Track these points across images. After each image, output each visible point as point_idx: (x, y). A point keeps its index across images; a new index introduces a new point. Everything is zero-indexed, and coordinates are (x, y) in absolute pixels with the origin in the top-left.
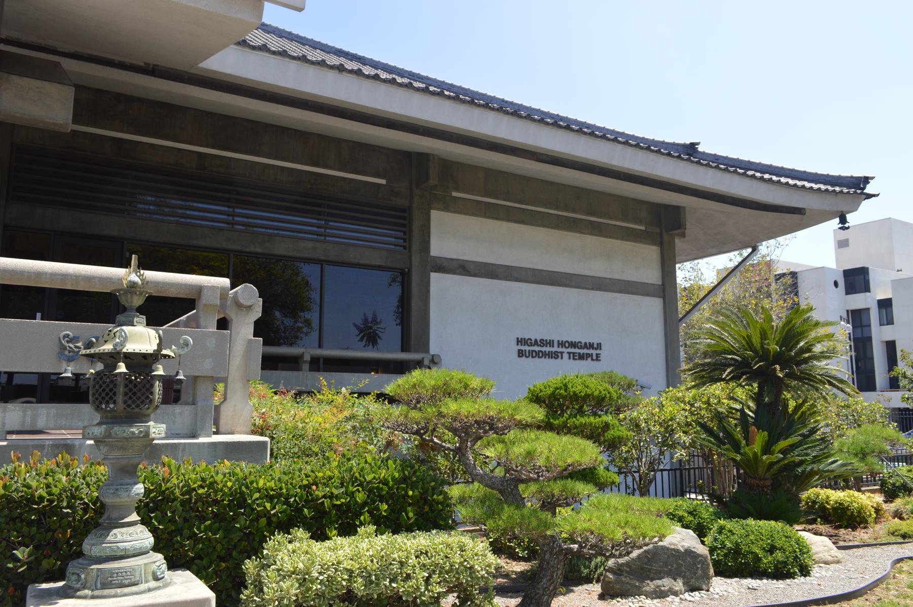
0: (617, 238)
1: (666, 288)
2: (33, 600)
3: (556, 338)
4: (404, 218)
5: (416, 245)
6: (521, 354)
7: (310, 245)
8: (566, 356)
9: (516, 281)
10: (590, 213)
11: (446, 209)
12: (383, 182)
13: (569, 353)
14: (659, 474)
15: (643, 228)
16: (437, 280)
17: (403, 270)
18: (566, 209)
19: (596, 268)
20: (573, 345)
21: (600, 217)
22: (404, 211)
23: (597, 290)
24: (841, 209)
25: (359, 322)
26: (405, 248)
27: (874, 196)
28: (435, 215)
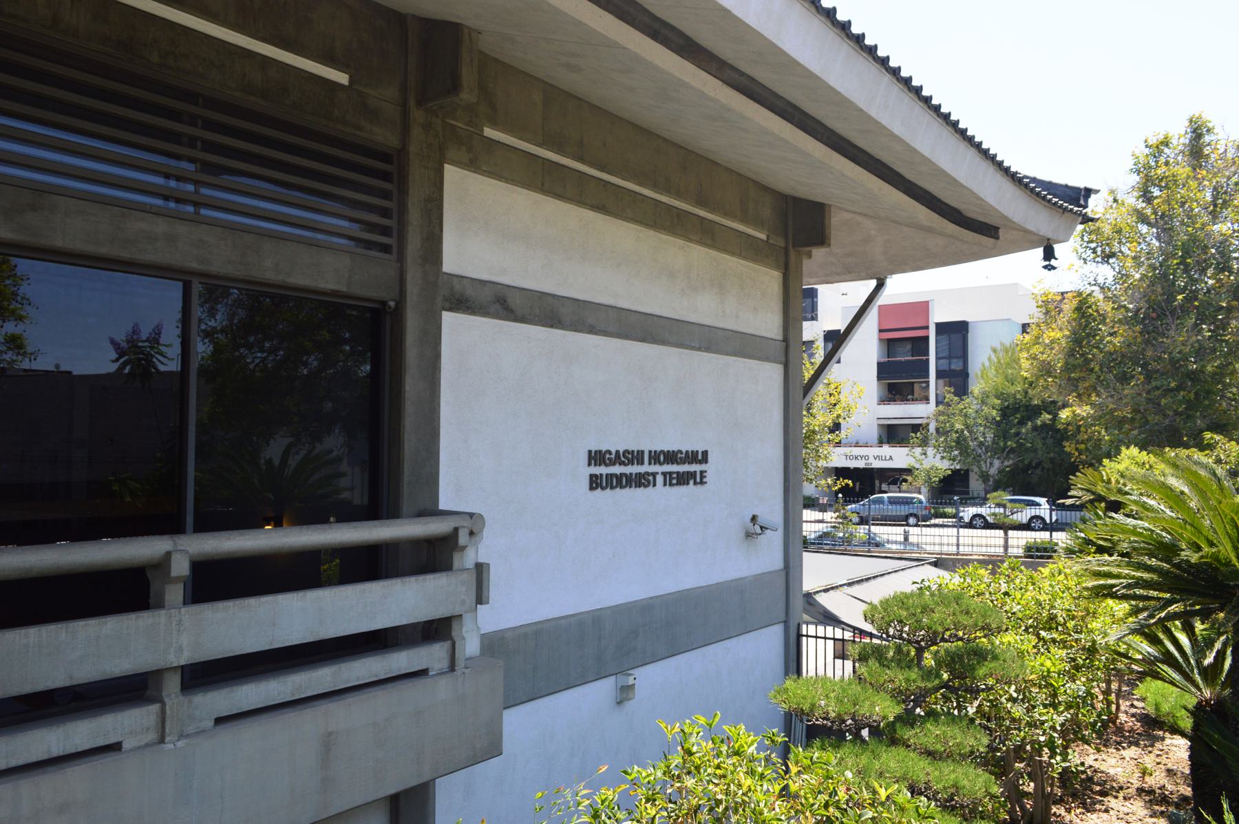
3: (647, 446)
4: (386, 176)
5: (414, 244)
6: (595, 483)
7: (160, 226)
8: (660, 479)
9: (590, 332)
10: (701, 202)
11: (472, 165)
12: (342, 78)
13: (664, 474)
15: (763, 236)
16: (459, 332)
17: (384, 303)
18: (667, 191)
19: (703, 309)
20: (671, 457)
21: (712, 211)
22: (385, 157)
24: (1050, 236)
25: (121, 337)
28: (452, 174)
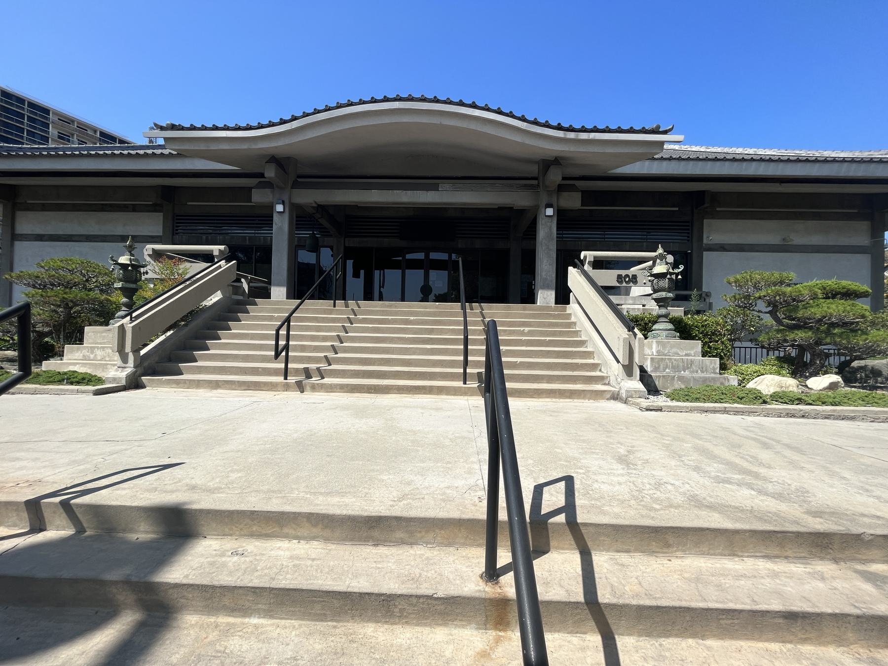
2: (839, 382)
14: (737, 350)
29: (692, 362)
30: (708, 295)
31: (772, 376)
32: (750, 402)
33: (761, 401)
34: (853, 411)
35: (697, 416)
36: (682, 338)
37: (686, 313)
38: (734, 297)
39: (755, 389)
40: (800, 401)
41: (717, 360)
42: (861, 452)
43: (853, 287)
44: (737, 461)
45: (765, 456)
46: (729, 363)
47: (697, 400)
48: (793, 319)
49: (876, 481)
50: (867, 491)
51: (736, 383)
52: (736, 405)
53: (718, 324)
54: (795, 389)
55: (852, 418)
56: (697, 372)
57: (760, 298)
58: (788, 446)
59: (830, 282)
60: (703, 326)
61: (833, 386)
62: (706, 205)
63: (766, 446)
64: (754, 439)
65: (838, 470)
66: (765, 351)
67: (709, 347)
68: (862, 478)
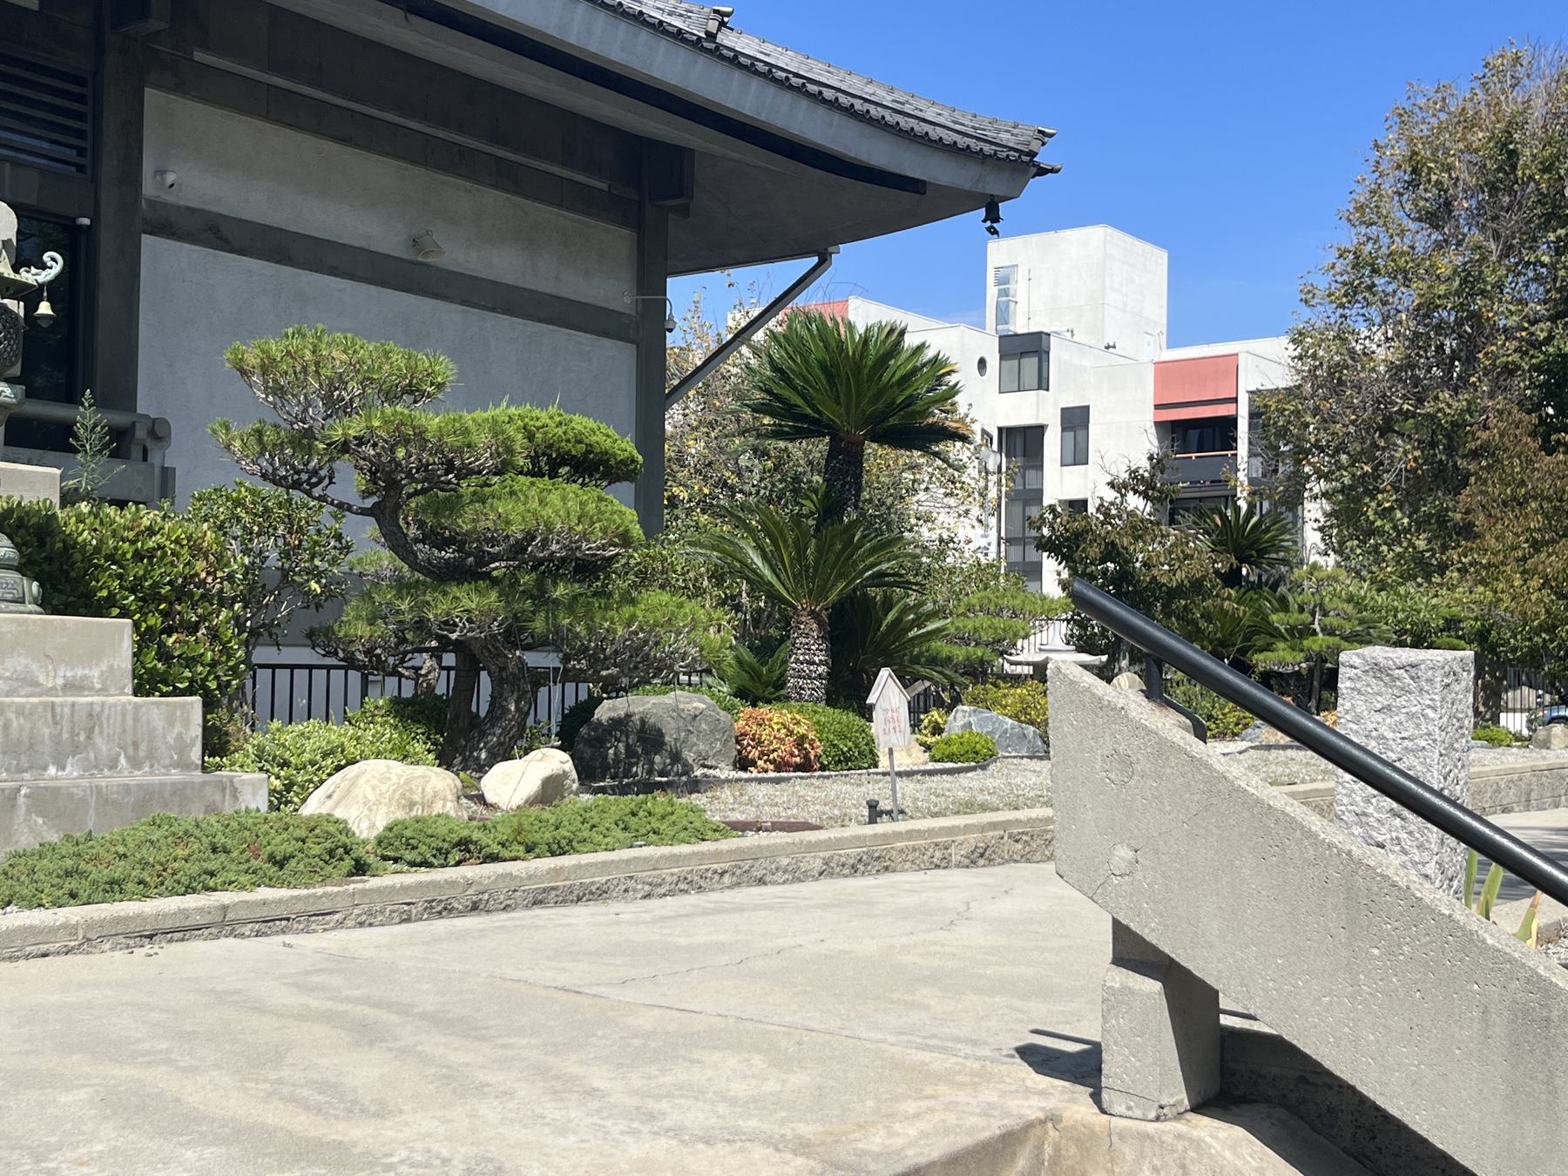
0: (550, 204)
1: (646, 327)
2: (565, 775)
5: (109, 166)
11: (179, 88)
14: (264, 675)
15: (603, 186)
22: (81, 81)
23: (504, 312)
26: (80, 168)
27: (1052, 171)
29: (93, 718)
30: (158, 432)
31: (380, 764)
32: (315, 874)
33: (348, 863)
34: (605, 865)
35: (114, 963)
36: (54, 602)
37: (68, 498)
38: (259, 433)
39: (328, 818)
40: (466, 849)
41: (196, 701)
42: (628, 995)
43: (598, 438)
44: (276, 1116)
45: (364, 1071)
46: (236, 726)
47: (114, 888)
48: (443, 544)
49: (667, 1079)
50: (651, 1117)
51: (260, 802)
52: (264, 893)
53: (197, 550)
54: (450, 808)
55: (599, 894)
56: (113, 765)
57: (345, 447)
58: (439, 1021)
59: (544, 417)
60: (138, 556)
61: (551, 790)
62: (155, 24)
63: (366, 1035)
64: (327, 1017)
65: (576, 1070)
66: (355, 676)
67: (164, 655)
68: (636, 1080)
